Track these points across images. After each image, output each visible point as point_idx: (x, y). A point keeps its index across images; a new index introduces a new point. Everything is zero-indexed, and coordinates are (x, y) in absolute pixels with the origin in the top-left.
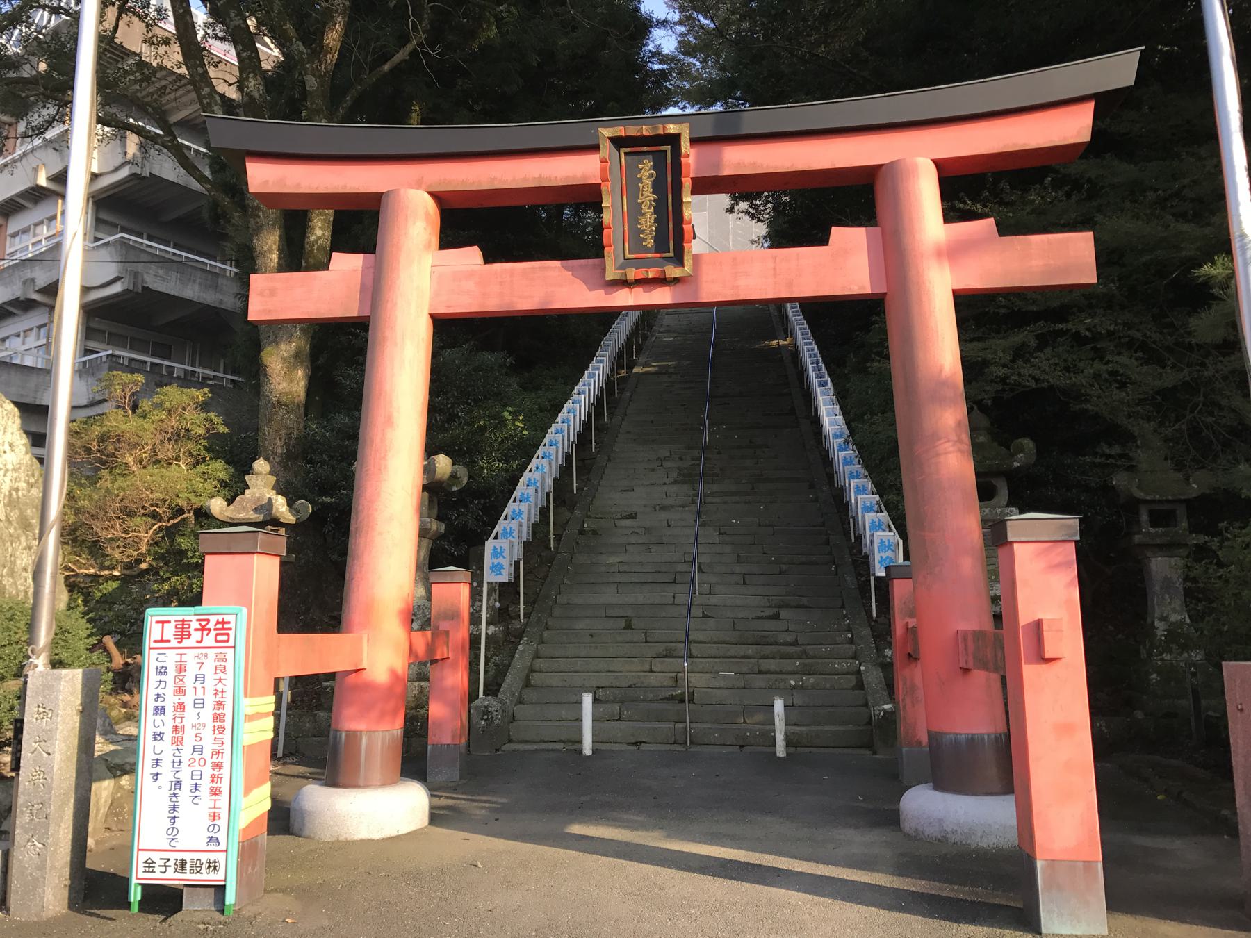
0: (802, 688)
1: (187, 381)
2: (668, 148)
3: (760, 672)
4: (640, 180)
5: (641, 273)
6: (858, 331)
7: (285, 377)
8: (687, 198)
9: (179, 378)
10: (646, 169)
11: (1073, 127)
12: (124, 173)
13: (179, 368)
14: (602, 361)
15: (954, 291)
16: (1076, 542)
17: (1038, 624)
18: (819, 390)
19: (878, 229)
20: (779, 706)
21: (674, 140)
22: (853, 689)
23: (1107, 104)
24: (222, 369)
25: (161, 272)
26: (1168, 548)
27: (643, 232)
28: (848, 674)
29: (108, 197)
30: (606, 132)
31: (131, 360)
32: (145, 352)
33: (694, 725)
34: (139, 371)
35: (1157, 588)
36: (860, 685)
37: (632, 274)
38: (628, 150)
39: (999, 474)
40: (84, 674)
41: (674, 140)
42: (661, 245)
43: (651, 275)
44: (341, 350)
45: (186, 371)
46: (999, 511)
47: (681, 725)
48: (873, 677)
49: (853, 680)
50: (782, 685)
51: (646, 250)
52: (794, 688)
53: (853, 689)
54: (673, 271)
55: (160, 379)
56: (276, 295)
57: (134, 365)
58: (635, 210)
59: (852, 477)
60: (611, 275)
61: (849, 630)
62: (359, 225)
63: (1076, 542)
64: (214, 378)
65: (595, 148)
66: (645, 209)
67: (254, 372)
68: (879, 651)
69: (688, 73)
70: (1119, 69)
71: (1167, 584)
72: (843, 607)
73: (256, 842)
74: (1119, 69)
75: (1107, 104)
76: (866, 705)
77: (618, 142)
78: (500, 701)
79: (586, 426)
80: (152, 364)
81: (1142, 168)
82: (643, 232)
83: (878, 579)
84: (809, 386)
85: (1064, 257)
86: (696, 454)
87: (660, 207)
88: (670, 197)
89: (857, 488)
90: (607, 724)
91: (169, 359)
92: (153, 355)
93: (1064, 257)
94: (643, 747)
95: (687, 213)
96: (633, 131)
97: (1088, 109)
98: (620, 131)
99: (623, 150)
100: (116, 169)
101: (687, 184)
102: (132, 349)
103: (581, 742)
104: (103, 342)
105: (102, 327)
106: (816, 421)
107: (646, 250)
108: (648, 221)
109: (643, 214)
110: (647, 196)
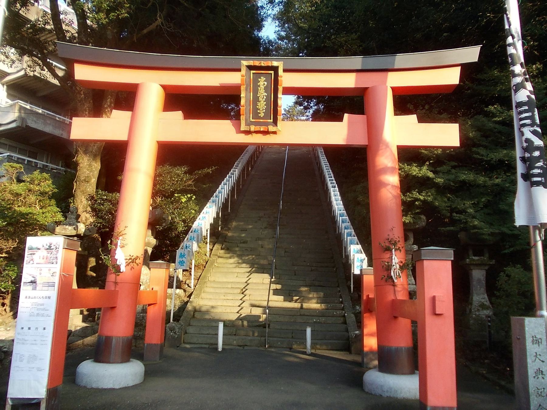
0: (319, 323)
1: (43, 169)
2: (272, 72)
3: (300, 315)
4: (259, 86)
5: (258, 128)
6: (352, 163)
7: (89, 169)
8: (280, 95)
9: (40, 168)
10: (262, 82)
11: (452, 77)
12: (22, 73)
13: (40, 163)
14: (235, 171)
15: (397, 146)
16: (452, 261)
17: (434, 299)
18: (332, 189)
19: (365, 116)
20: (309, 331)
21: (276, 69)
22: (342, 323)
23: (467, 69)
24: (60, 165)
25: (35, 119)
26: (479, 265)
27: (259, 110)
28: (339, 317)
29: (13, 84)
30: (245, 63)
31: (18, 158)
32: (25, 155)
33: (269, 338)
34: (21, 163)
35: (475, 283)
36: (345, 323)
37: (253, 128)
38: (254, 72)
39: (410, 230)
40: (514, 221)
41: (276, 69)
42: (267, 116)
43: (262, 130)
44: (113, 158)
45: (43, 165)
46: (409, 247)
47: (263, 339)
48: (351, 318)
49: (342, 319)
50: (311, 321)
51: (260, 118)
52: (315, 322)
53: (342, 323)
54: (271, 128)
55: (30, 168)
56: (84, 128)
57: (20, 161)
58: (256, 100)
59: (346, 228)
60: (243, 127)
61: (341, 297)
62: (125, 98)
63: (452, 261)
64: (56, 169)
65: (239, 70)
66: (260, 99)
67: (71, 166)
68: (354, 307)
69: (281, 49)
70: (471, 54)
71: (479, 280)
72: (338, 287)
73: (57, 389)
74: (471, 54)
75: (467, 69)
76: (347, 331)
77: (250, 68)
78: (180, 324)
79: (226, 200)
80: (28, 161)
81: (475, 100)
82: (259, 110)
83: (355, 276)
84: (327, 188)
85: (446, 135)
86: (276, 215)
87: (268, 100)
88: (272, 100)
89: (347, 234)
90: (230, 337)
91: (36, 159)
92: (29, 157)
93: (446, 135)
94: (246, 348)
95: (280, 102)
96: (257, 63)
97: (459, 68)
98: (251, 63)
99: (252, 72)
100: (18, 71)
101: (280, 89)
102: (19, 153)
103: (217, 344)
104: (5, 149)
105: (6, 142)
106: (329, 204)
107: (260, 118)
108: (262, 105)
109: (259, 101)
110: (262, 94)
